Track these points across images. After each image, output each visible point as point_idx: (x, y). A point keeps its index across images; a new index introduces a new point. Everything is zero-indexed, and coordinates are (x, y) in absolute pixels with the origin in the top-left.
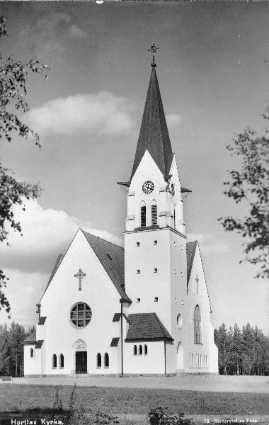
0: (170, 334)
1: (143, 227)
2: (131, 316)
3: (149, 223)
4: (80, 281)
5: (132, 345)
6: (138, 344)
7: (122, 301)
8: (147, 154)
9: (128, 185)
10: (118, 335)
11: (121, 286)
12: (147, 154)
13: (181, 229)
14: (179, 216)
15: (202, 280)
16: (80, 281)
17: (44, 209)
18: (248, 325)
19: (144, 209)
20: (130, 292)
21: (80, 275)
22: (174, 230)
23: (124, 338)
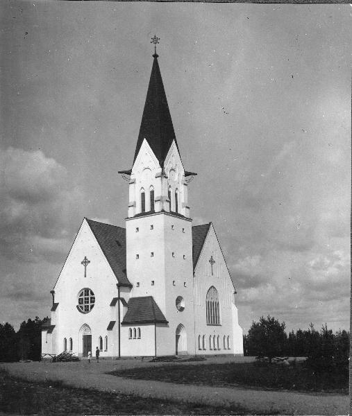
0: (164, 313)
1: (143, 214)
2: (132, 300)
3: (148, 209)
6: (132, 328)
7: (119, 286)
8: (145, 139)
9: (129, 173)
10: (115, 319)
12: (145, 139)
13: (182, 211)
14: (182, 199)
15: (218, 257)
19: (143, 195)
20: (131, 276)
21: (86, 262)
22: (176, 214)
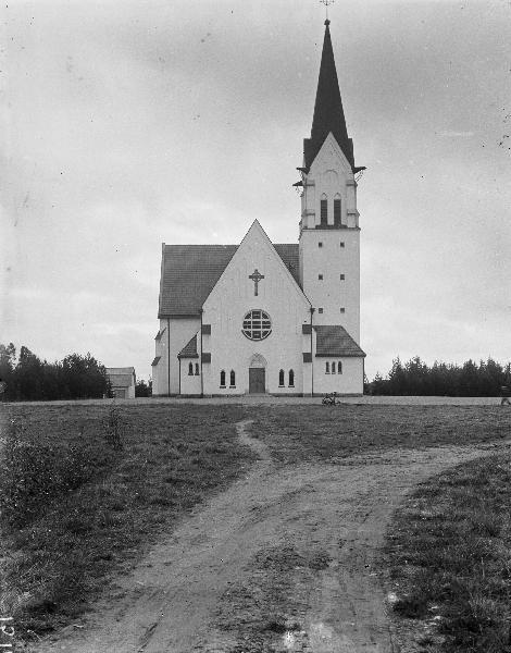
1: (324, 226)
3: (331, 221)
4: (256, 285)
5: (323, 361)
8: (330, 135)
11: (351, 159)
12: (330, 135)
16: (256, 285)
17: (75, 359)
18: (471, 361)
23: (314, 352)
